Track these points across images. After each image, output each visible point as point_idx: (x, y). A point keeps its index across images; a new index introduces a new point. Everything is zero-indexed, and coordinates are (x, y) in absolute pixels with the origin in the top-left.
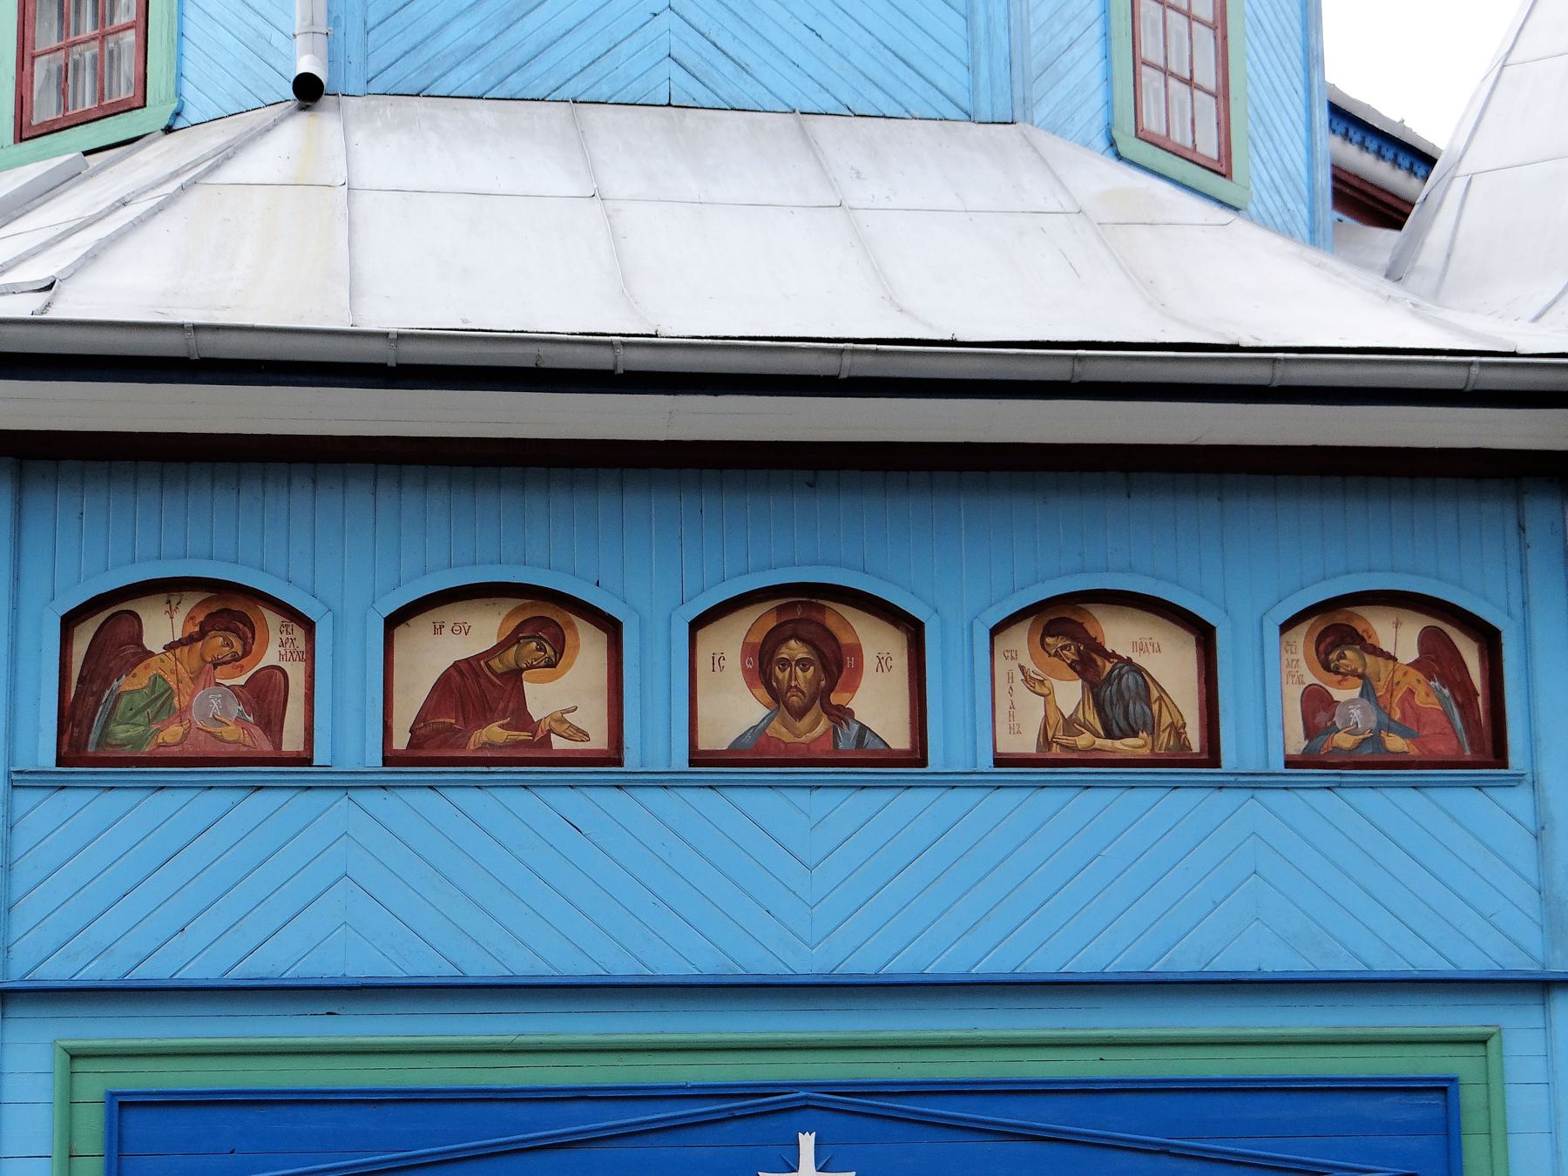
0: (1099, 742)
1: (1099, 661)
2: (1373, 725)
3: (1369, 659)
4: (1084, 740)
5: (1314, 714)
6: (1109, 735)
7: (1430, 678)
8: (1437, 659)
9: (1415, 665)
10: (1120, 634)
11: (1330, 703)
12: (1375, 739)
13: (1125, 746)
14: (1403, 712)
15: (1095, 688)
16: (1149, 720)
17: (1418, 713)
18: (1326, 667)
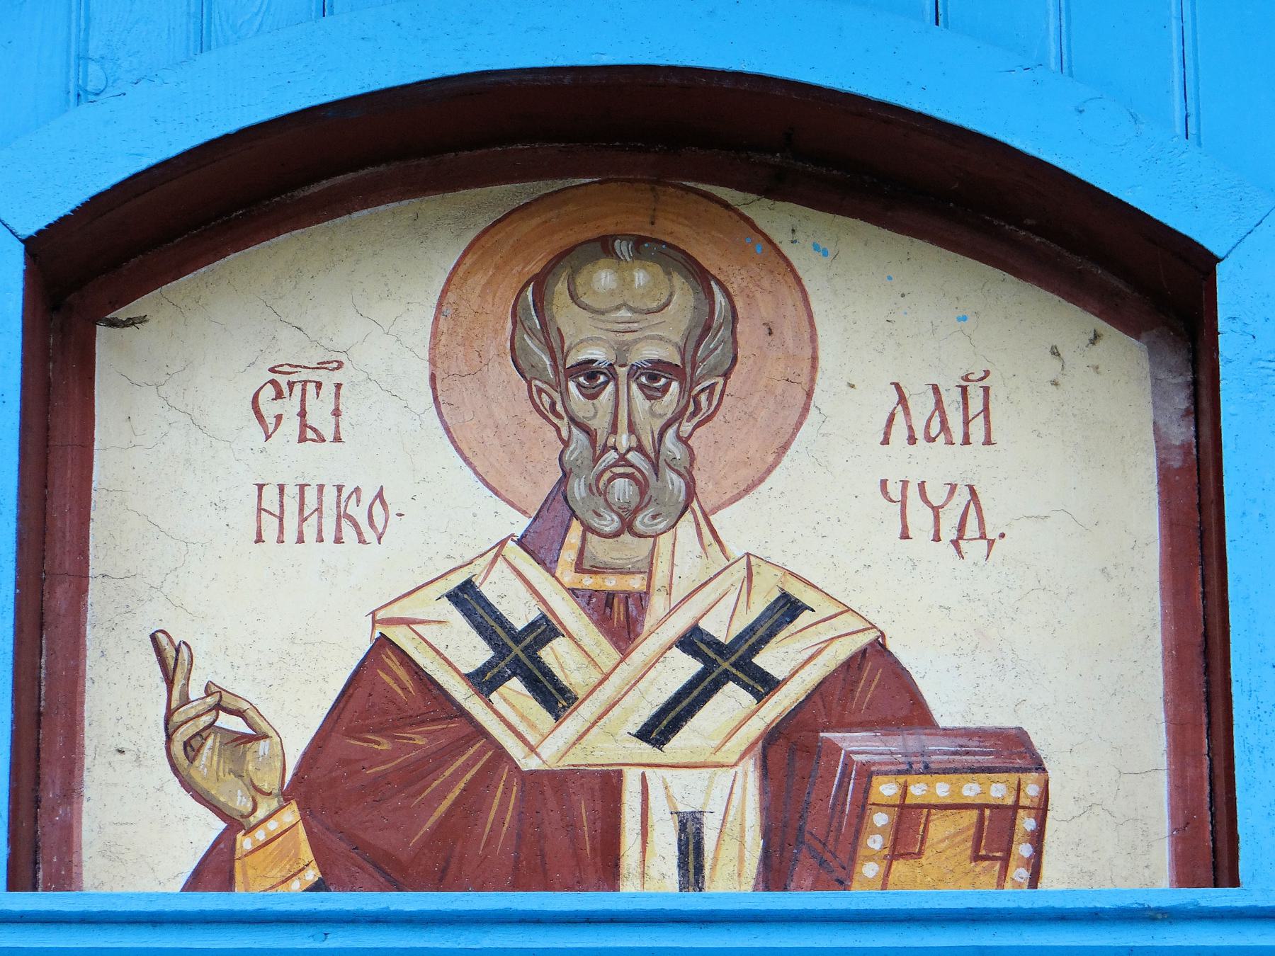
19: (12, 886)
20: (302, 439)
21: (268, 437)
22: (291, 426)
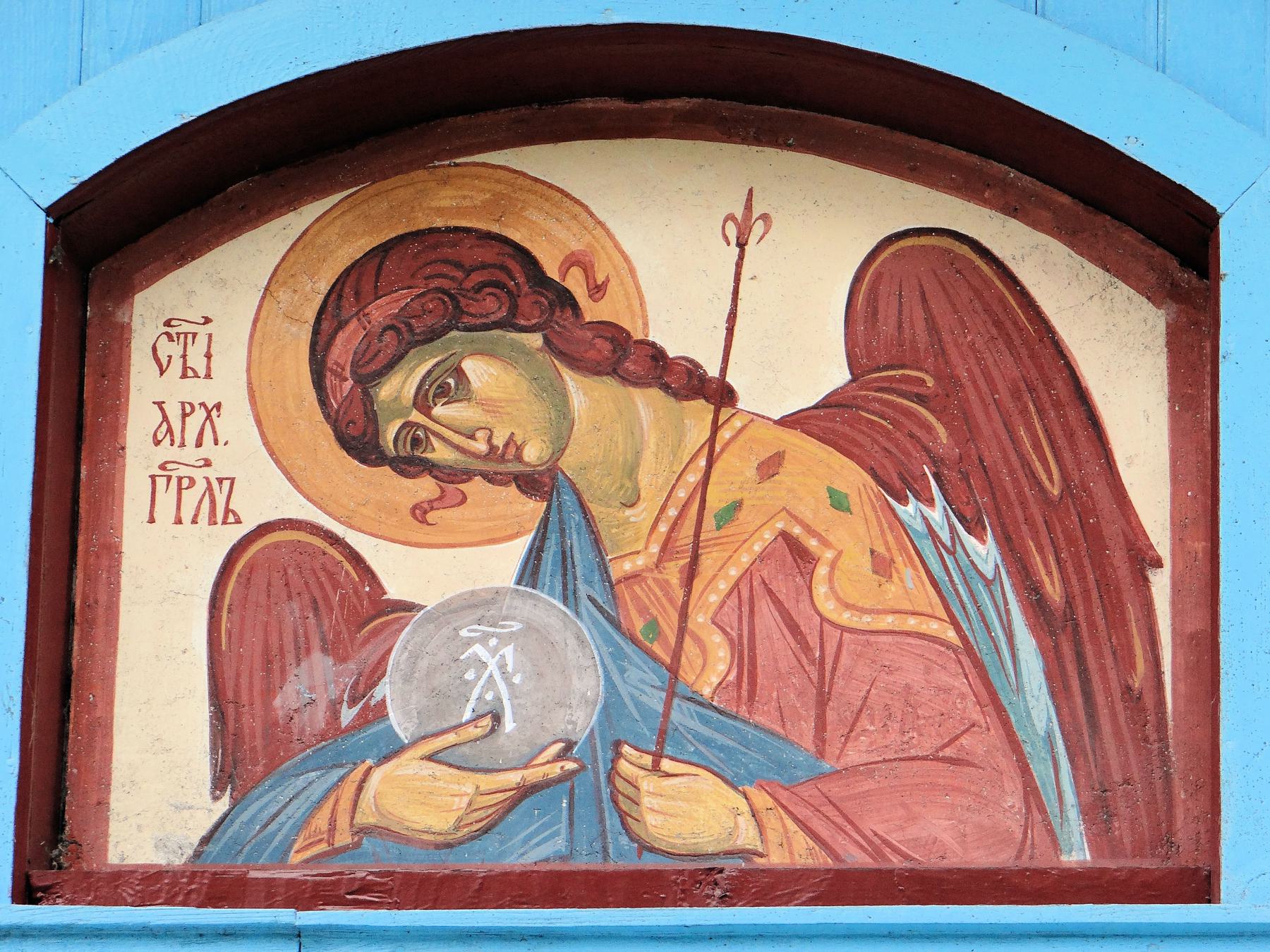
2: (581, 721)
3: (584, 393)
5: (273, 668)
7: (899, 484)
8: (947, 394)
9: (825, 421)
11: (363, 613)
12: (589, 778)
14: (745, 657)
17: (819, 657)
18: (361, 444)
19: (26, 892)
20: (184, 376)
21: (162, 373)
22: (177, 365)
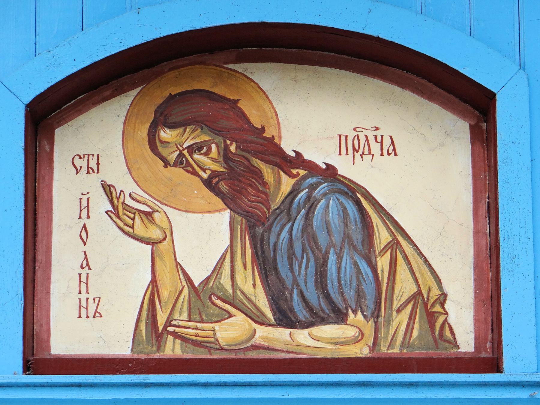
0: (265, 334)
1: (268, 173)
4: (232, 331)
6: (285, 319)
10: (310, 117)
13: (311, 341)
15: (255, 225)
16: (369, 289)
